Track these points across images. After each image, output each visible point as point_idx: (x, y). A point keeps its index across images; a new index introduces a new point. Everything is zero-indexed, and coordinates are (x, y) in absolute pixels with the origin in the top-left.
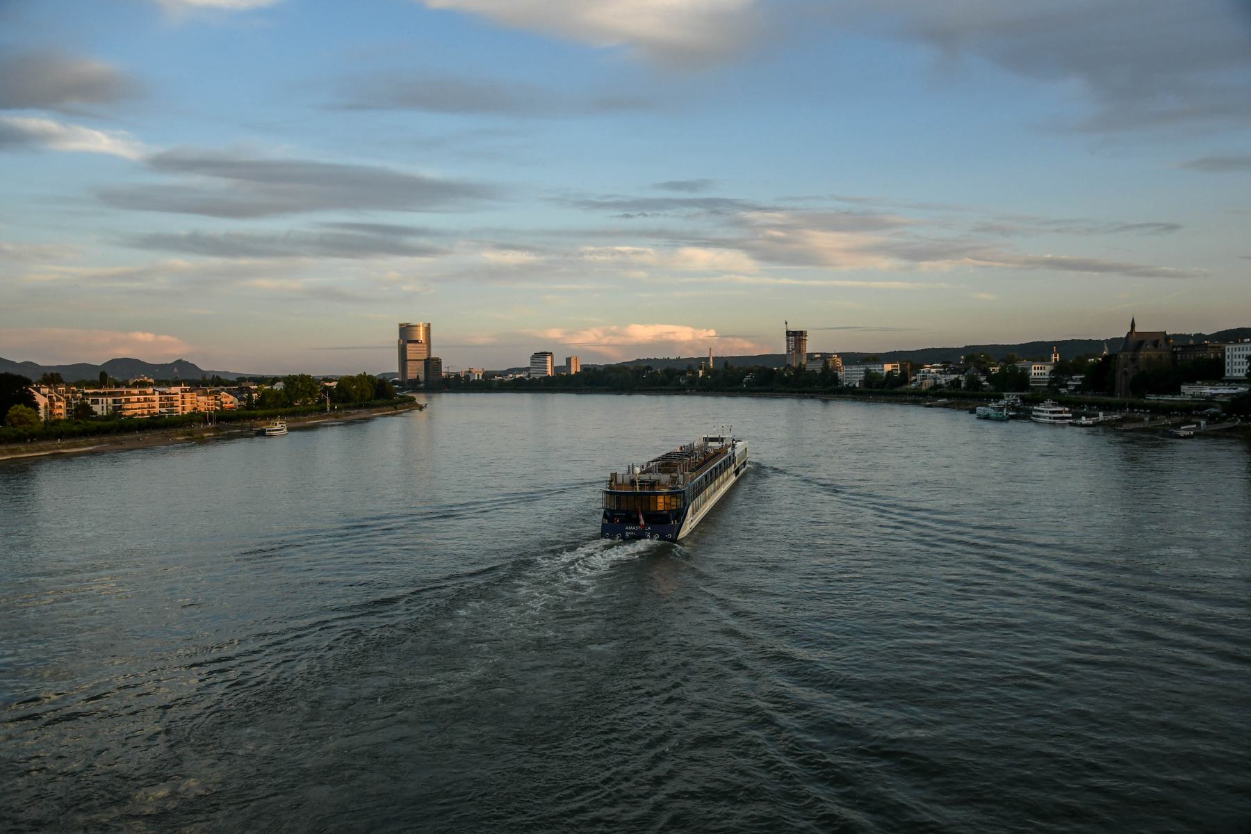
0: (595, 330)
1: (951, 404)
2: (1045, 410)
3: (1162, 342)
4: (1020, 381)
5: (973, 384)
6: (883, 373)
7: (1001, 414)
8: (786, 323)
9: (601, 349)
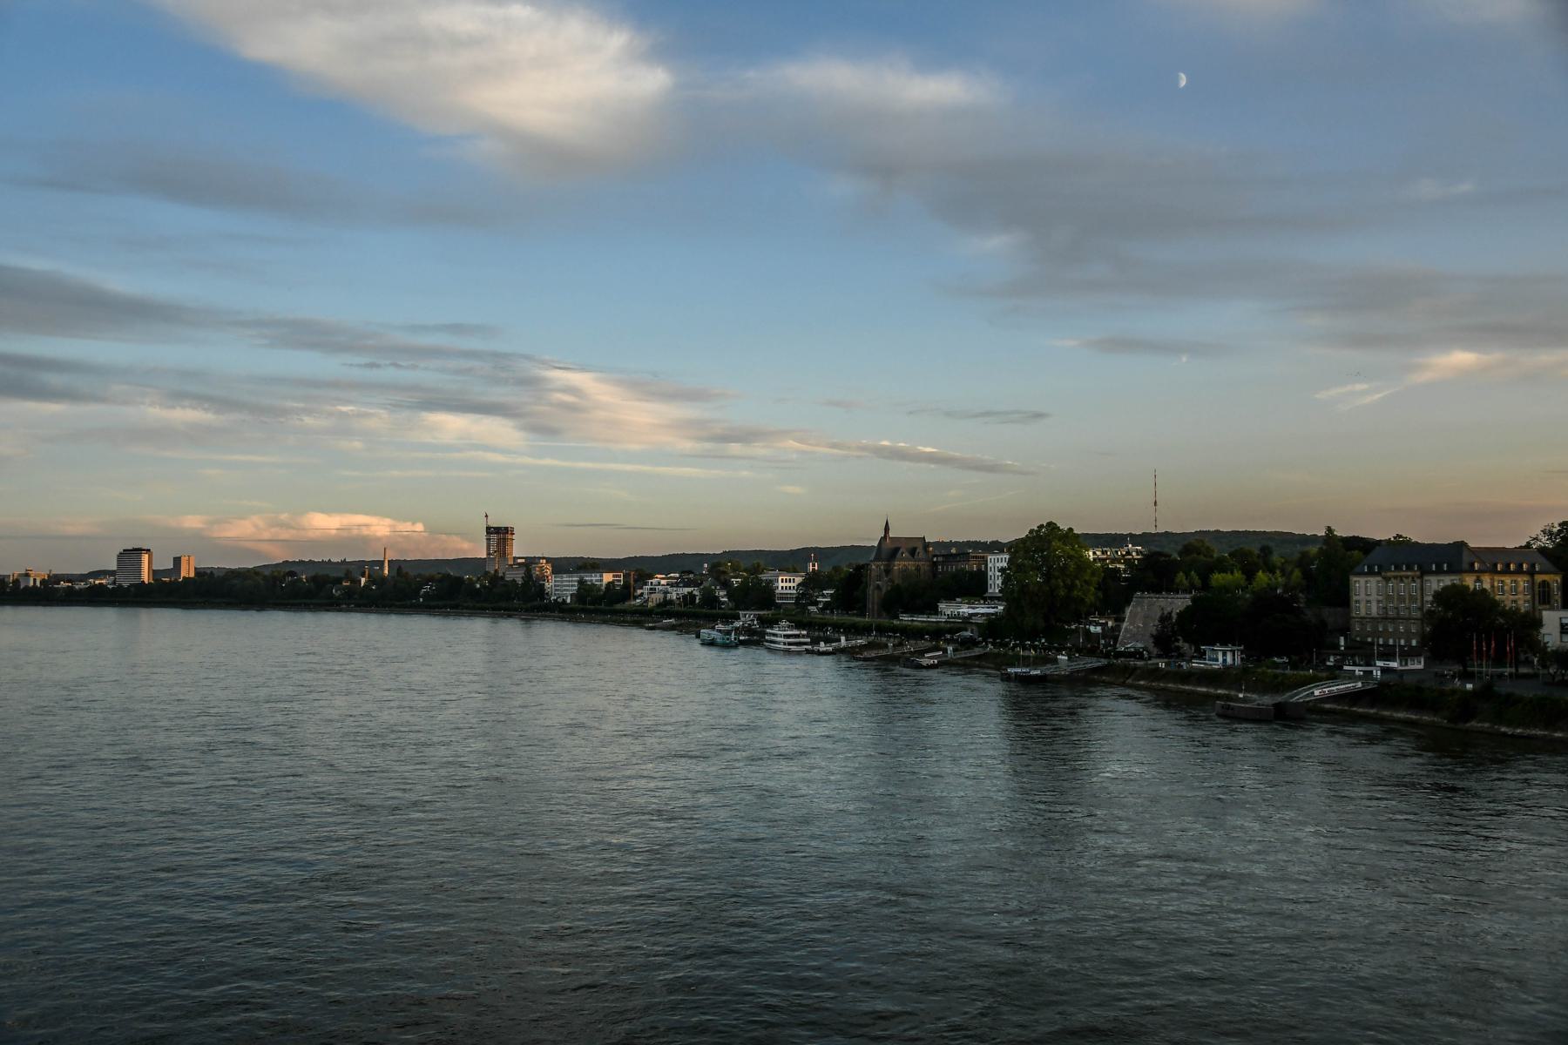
0: (255, 519)
1: (680, 625)
2: (781, 633)
3: (920, 546)
4: (762, 597)
5: (710, 600)
6: (601, 585)
7: (728, 639)
8: (486, 516)
9: (265, 547)
